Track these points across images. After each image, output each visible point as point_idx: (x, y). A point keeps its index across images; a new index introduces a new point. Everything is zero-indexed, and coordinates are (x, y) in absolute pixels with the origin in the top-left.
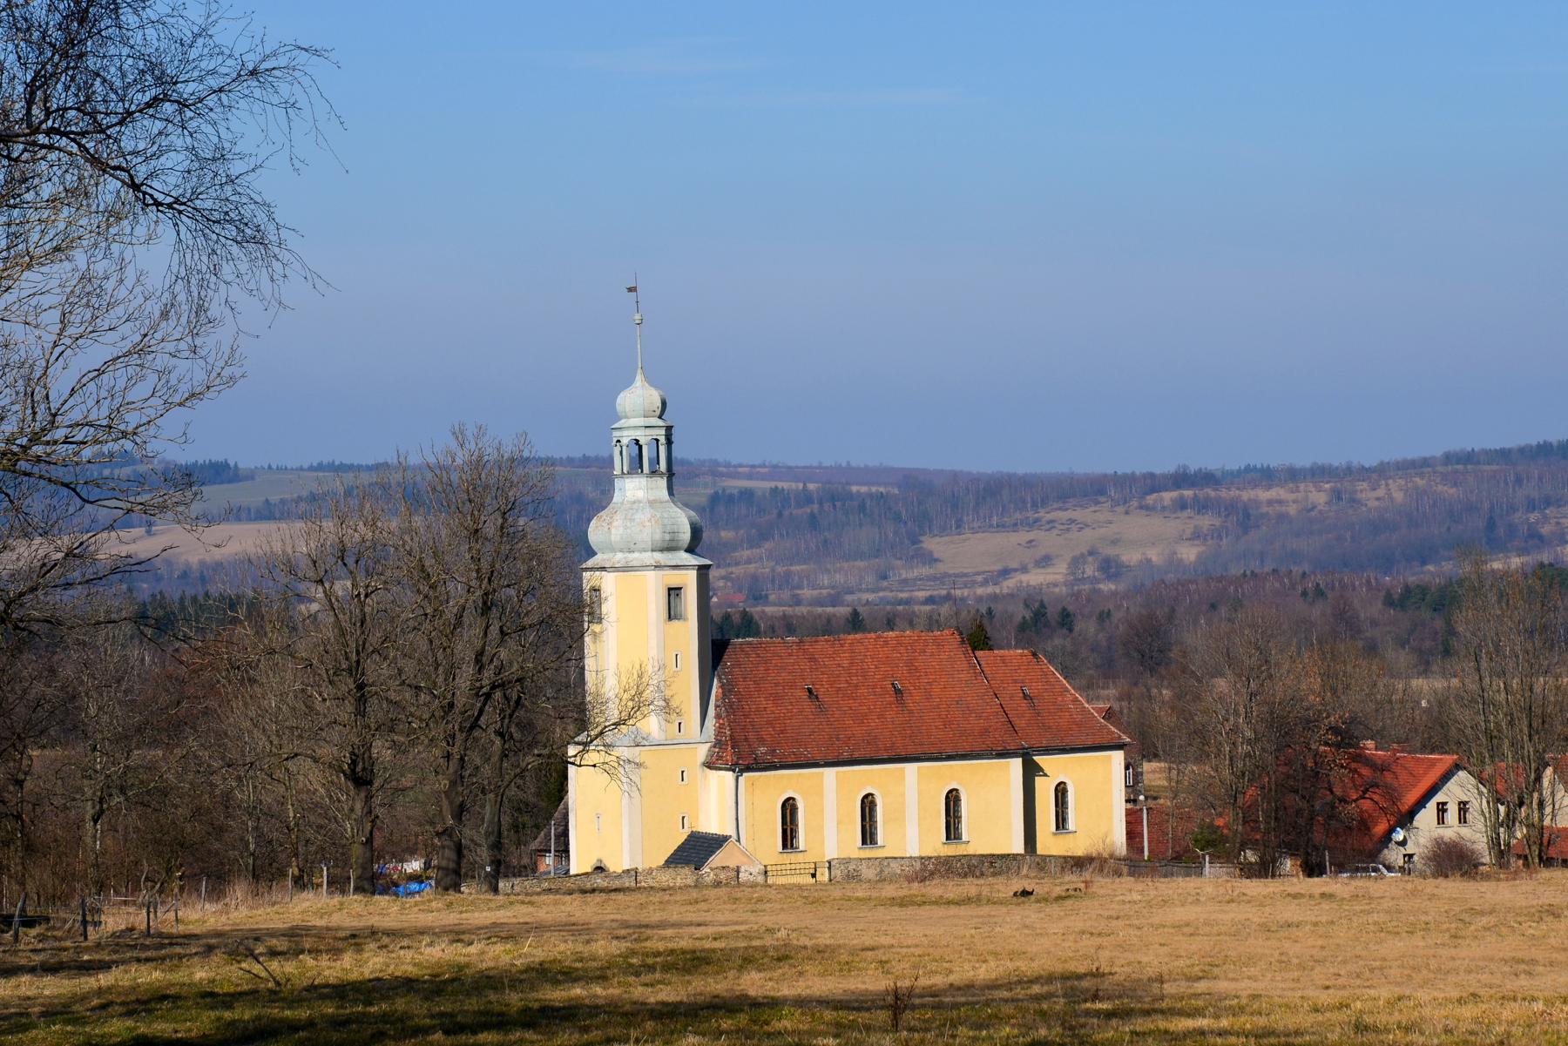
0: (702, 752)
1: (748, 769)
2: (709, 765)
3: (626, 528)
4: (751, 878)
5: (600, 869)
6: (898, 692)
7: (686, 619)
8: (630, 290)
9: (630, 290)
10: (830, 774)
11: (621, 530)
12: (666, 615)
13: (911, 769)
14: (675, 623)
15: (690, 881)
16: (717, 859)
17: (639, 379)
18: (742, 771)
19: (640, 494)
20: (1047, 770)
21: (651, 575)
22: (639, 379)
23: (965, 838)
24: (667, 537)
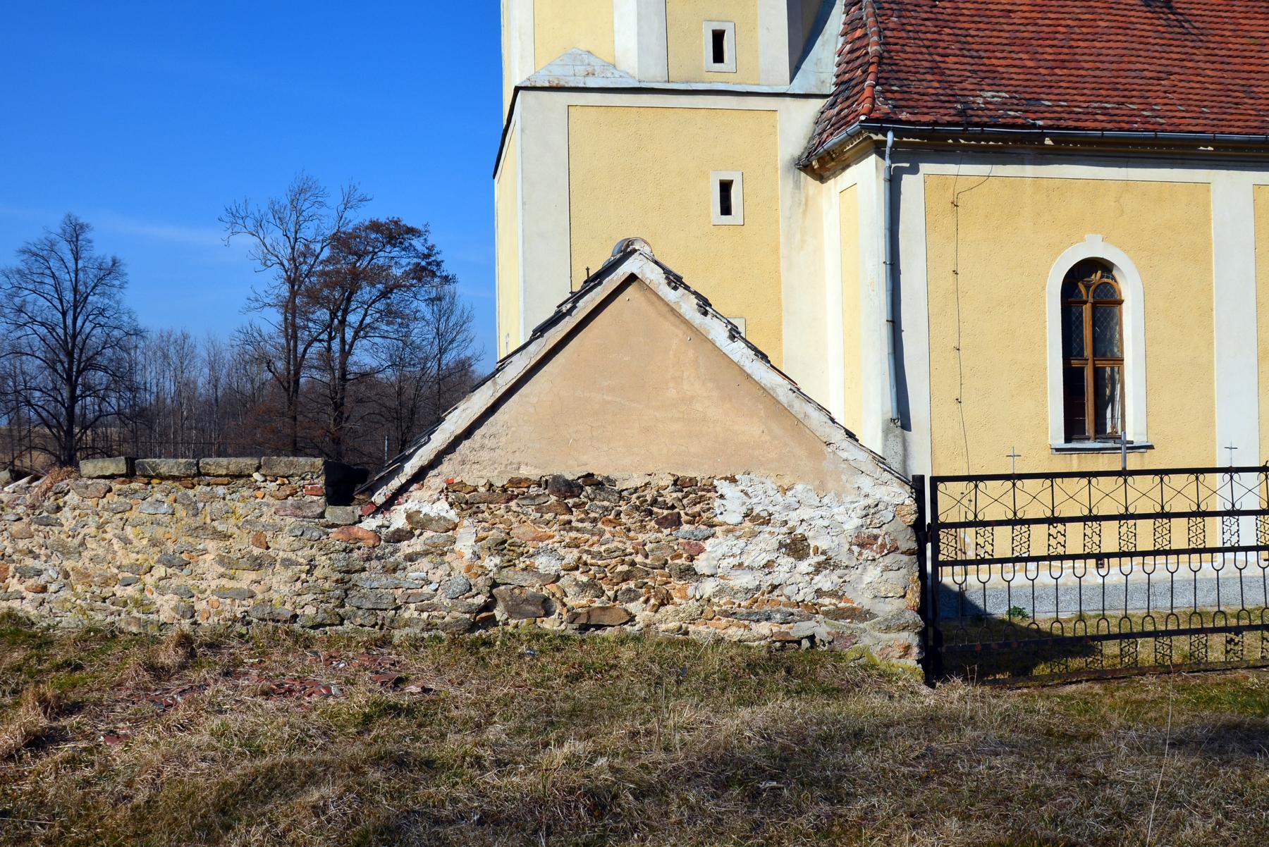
0: (796, 124)
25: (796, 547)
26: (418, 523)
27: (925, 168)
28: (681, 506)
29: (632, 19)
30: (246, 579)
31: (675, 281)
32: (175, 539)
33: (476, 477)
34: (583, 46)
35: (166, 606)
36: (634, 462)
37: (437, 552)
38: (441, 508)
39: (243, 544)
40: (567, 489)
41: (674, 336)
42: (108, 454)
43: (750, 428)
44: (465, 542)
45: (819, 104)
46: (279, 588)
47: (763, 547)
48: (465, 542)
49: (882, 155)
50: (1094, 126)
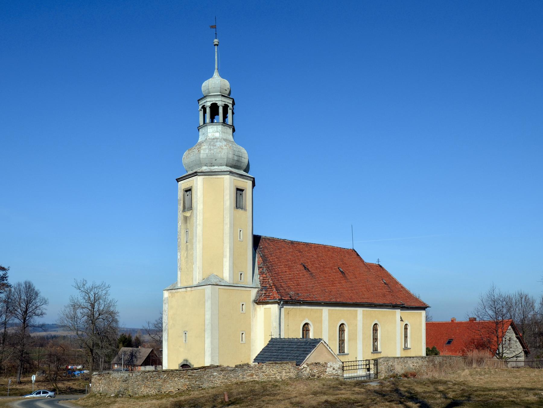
0: (253, 293)
1: (287, 303)
2: (258, 302)
3: (210, 150)
4: (334, 372)
5: (185, 366)
6: (342, 272)
7: (245, 210)
8: (212, 27)
9: (212, 27)
10: (325, 311)
11: (207, 151)
12: (234, 205)
13: (360, 311)
14: (240, 211)
15: (154, 369)
16: (312, 357)
17: (216, 75)
18: (283, 305)
19: (217, 135)
20: (430, 305)
21: (227, 177)
22: (216, 75)
23: (346, 352)
24: (236, 158)
25: (334, 369)
26: (304, 367)
27: (284, 307)
28: (325, 365)
29: (228, 271)
30: (288, 374)
31: (325, 343)
32: (280, 370)
33: (309, 363)
34: (215, 274)
35: (278, 378)
36: (322, 362)
37: (305, 370)
38: (306, 366)
39: (288, 370)
40: (316, 364)
41: (324, 348)
42: (80, 365)
43: (330, 357)
44: (308, 370)
45: (257, 289)
46: (292, 375)
47: (331, 369)
48: (308, 370)
49: (279, 305)
50: (309, 299)
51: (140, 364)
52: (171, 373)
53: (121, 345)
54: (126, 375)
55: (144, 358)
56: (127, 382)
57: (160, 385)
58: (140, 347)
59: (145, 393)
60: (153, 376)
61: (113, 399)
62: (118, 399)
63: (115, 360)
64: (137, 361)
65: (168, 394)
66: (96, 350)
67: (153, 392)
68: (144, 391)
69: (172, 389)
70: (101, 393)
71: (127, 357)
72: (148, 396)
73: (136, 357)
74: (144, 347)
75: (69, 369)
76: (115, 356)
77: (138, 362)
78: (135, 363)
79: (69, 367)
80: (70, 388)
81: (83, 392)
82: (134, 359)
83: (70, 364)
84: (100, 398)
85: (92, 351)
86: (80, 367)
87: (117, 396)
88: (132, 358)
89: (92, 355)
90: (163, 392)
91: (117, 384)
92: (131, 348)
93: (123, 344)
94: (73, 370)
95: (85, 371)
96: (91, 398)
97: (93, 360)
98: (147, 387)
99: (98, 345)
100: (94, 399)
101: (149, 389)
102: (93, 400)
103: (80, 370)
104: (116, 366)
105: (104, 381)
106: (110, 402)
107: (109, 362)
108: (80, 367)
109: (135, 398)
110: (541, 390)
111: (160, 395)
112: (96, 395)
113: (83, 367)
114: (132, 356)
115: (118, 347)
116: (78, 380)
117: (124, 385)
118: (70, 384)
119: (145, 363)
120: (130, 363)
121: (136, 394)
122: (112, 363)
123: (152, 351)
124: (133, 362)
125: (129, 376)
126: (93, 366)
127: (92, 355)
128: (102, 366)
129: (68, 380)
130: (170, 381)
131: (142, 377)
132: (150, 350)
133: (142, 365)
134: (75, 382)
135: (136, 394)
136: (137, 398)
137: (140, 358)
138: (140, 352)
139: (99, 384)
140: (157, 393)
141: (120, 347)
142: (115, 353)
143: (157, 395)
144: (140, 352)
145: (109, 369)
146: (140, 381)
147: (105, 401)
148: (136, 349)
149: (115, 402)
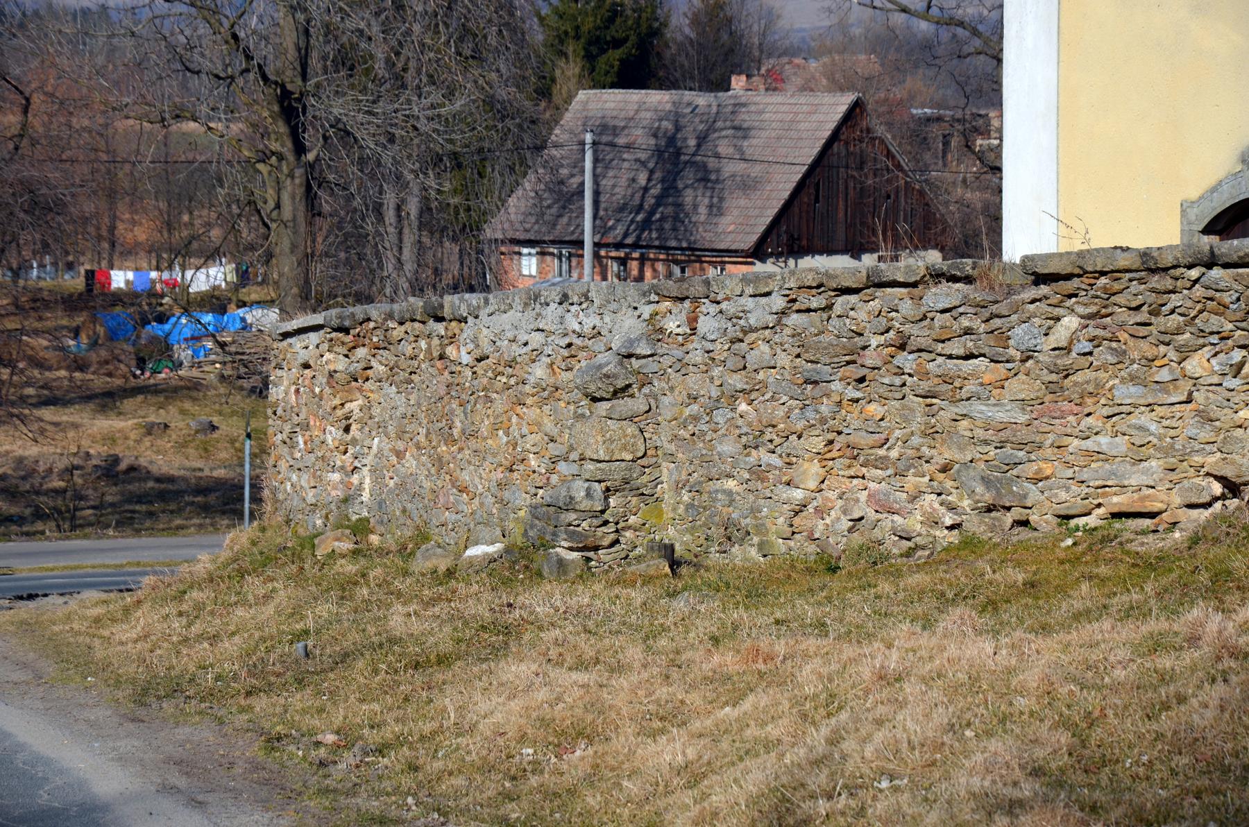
42: (211, 256)
51: (748, 241)
52: (1136, 292)
53: (569, 69)
54: (626, 326)
55: (783, 185)
56: (637, 404)
57: (1003, 436)
58: (738, 83)
59: (832, 527)
60: (920, 335)
61: (479, 603)
62: (540, 600)
63: (516, 209)
64: (716, 210)
65: (1100, 540)
66: (334, 105)
67: (925, 513)
68: (827, 500)
69: (1144, 482)
70: (360, 529)
71: (624, 180)
72: (873, 560)
73: (706, 178)
74: (775, 82)
75: (118, 298)
76: (517, 169)
77: (727, 223)
78: (705, 236)
79: (120, 279)
80: (110, 470)
81: (223, 500)
82: (694, 198)
83: (120, 252)
84: (345, 587)
85: (290, 108)
86: (210, 277)
87: (523, 562)
88: (670, 189)
89: (300, 149)
90: (1043, 520)
91: (533, 427)
92: (657, 98)
93: (590, 57)
94: (147, 307)
95: (253, 316)
96: (254, 586)
97: (310, 197)
98: (853, 453)
99: (348, 61)
100: (284, 595)
101: (877, 482)
102: (266, 608)
103: (216, 302)
104: (529, 264)
105: (390, 399)
106: (442, 639)
107: (466, 227)
108: (210, 277)
109: (722, 587)
110: (9, 519)
111: (1008, 556)
112: (310, 542)
113: (244, 277)
114: (678, 163)
115: (544, 91)
116: (192, 388)
117: (601, 435)
118: (96, 433)
119: (789, 235)
120: (656, 233)
121: (732, 534)
122: (488, 233)
123: (856, 110)
124: (679, 217)
125: (656, 333)
126: (308, 258)
127: (300, 149)
128: (401, 251)
129: (107, 400)
130: (1127, 393)
131: (802, 348)
132: (841, 104)
133: (758, 252)
134: (171, 414)
135: (732, 534)
136: (753, 589)
137: (747, 185)
138: (742, 132)
139: (359, 429)
140: (976, 525)
141: (559, 91)
142: (519, 134)
143: (970, 544)
144: (742, 132)
145: (475, 282)
146: (753, 401)
147: (398, 620)
148: (703, 100)
149: (500, 636)
